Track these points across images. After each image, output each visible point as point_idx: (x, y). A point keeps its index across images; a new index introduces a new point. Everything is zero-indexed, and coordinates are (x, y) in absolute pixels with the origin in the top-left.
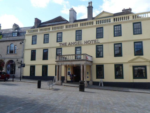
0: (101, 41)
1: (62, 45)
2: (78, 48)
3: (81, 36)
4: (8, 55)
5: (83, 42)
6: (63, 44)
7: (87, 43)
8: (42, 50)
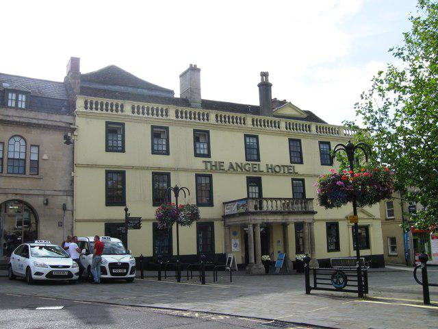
0: (299, 168)
2: (254, 182)
3: (248, 148)
6: (214, 164)
7: (273, 170)
8: (102, 175)
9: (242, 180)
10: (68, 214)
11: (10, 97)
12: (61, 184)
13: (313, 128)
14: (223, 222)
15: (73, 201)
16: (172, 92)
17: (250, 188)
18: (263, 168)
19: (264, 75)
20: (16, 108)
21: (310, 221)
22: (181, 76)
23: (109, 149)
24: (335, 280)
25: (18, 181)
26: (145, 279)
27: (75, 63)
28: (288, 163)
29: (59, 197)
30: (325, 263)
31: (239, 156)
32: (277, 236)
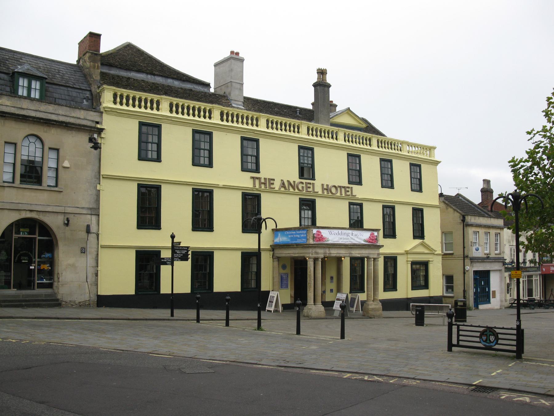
1: (261, 183)
4: (14, 191)
6: (263, 181)
9: (294, 203)
10: (92, 237)
11: (21, 83)
13: (374, 142)
14: (271, 253)
15: (99, 220)
16: (208, 85)
17: (303, 212)
20: (28, 97)
21: (375, 256)
22: (216, 65)
23: (142, 157)
24: (484, 338)
26: (203, 324)
28: (346, 184)
29: (83, 216)
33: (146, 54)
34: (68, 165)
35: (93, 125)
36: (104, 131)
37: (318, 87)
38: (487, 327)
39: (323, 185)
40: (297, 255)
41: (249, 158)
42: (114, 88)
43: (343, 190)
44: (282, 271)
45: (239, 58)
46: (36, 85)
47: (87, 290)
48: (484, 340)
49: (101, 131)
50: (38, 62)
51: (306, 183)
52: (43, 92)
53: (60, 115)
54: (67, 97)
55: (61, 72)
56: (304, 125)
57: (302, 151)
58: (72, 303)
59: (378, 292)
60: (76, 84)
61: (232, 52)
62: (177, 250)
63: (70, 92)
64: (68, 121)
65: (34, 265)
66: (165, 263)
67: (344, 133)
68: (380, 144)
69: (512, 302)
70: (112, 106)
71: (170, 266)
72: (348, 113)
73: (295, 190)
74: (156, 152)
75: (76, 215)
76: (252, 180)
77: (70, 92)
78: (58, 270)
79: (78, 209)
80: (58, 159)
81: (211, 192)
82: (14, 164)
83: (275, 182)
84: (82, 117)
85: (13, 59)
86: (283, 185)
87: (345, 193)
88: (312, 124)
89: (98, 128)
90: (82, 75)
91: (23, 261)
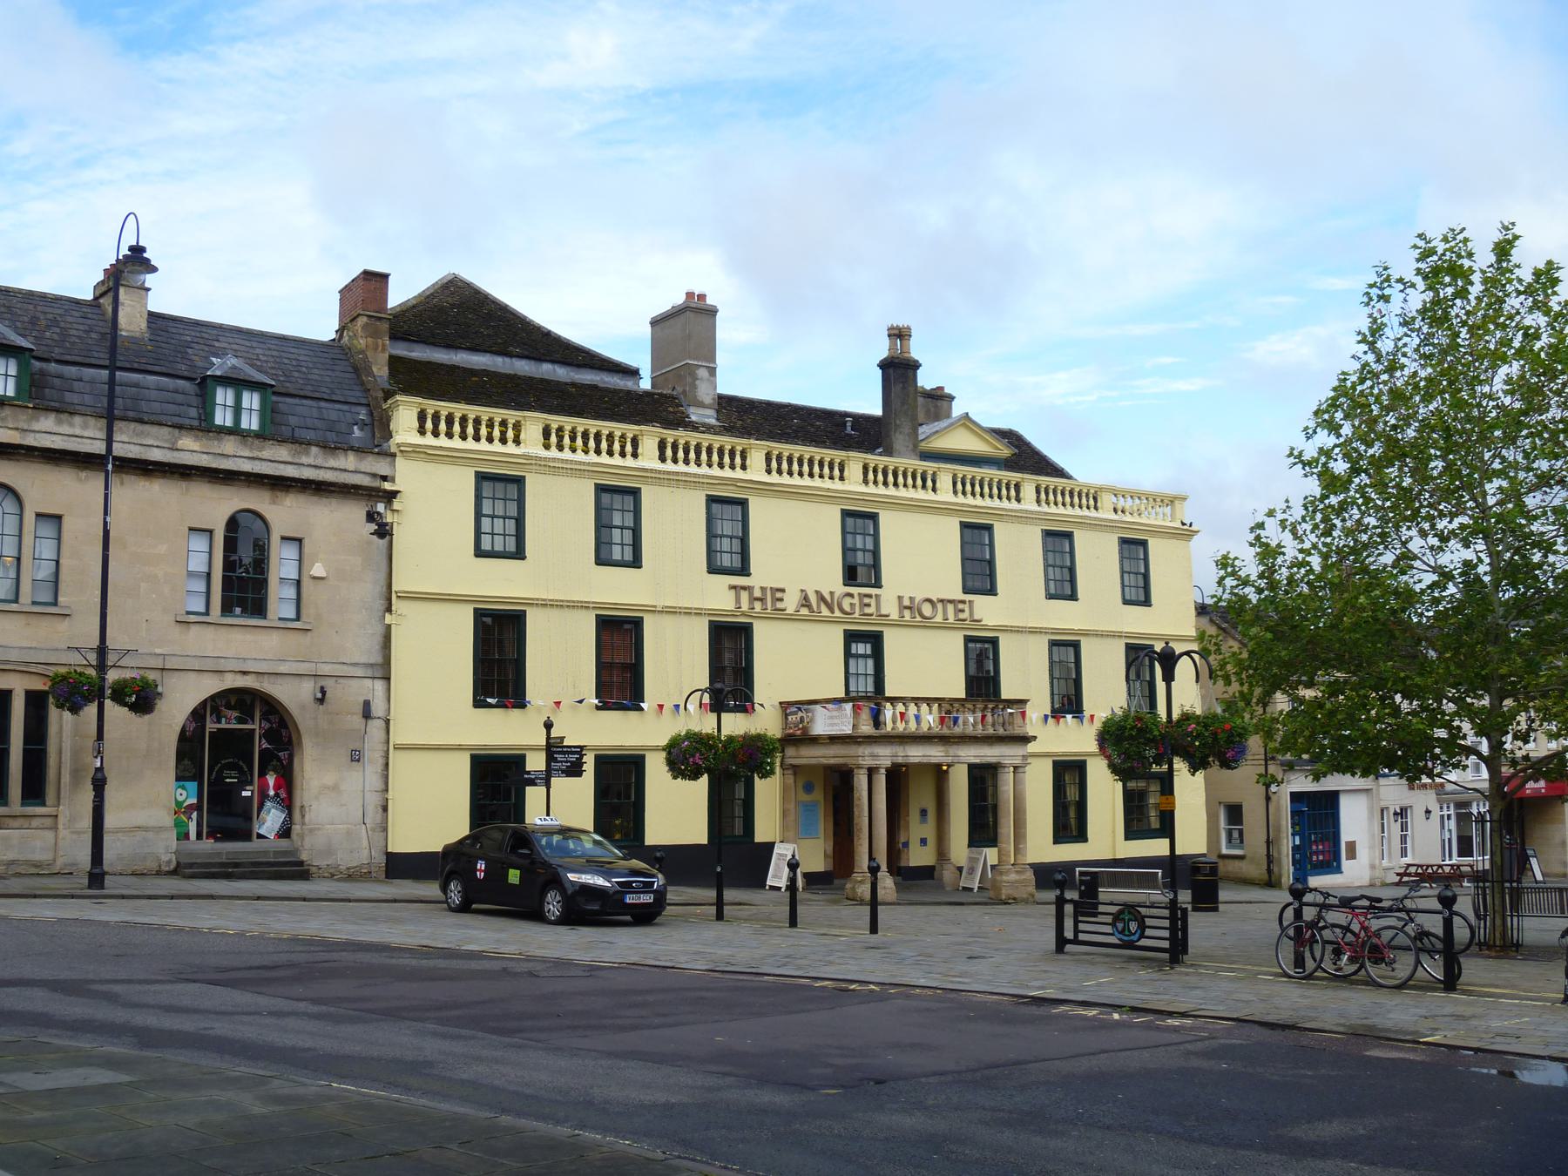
1: (753, 599)
4: (209, 632)
5: (888, 598)
6: (757, 593)
7: (916, 614)
10: (376, 727)
11: (219, 399)
12: (362, 649)
15: (389, 690)
16: (634, 373)
18: (890, 608)
19: (899, 334)
21: (1017, 762)
22: (656, 322)
24: (1120, 926)
25: (250, 637)
27: (136, 261)
29: (354, 682)
30: (1047, 875)
31: (947, 579)
32: (920, 796)
33: (494, 302)
34: (323, 574)
35: (376, 483)
36: (399, 495)
37: (891, 371)
38: (1124, 904)
39: (900, 598)
40: (832, 761)
41: (726, 541)
42: (420, 400)
43: (950, 608)
44: (805, 797)
45: (704, 307)
46: (251, 400)
47: (365, 843)
48: (1120, 929)
49: (391, 496)
50: (255, 344)
51: (859, 594)
52: (269, 413)
53: (303, 465)
54: (318, 424)
55: (303, 363)
56: (855, 462)
57: (850, 521)
58: (331, 871)
59: (1026, 843)
60: (338, 392)
61: (690, 295)
62: (559, 753)
63: (324, 410)
64: (321, 478)
65: (251, 788)
66: (532, 783)
67: (951, 475)
68: (1043, 496)
69: (1402, 871)
70: (417, 439)
71: (544, 789)
72: (964, 425)
73: (833, 612)
74: (514, 538)
75: (341, 680)
76: (733, 591)
77: (324, 410)
78: (302, 797)
79: (345, 667)
80: (300, 561)
81: (637, 624)
82: (209, 575)
83: (785, 596)
84: (351, 468)
85: (201, 341)
86: (805, 602)
87: (956, 615)
88: (873, 459)
89: (385, 491)
90: (350, 369)
91: (228, 780)
